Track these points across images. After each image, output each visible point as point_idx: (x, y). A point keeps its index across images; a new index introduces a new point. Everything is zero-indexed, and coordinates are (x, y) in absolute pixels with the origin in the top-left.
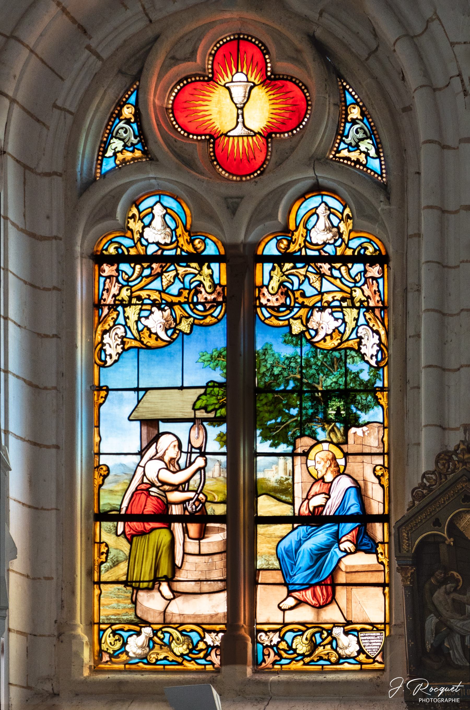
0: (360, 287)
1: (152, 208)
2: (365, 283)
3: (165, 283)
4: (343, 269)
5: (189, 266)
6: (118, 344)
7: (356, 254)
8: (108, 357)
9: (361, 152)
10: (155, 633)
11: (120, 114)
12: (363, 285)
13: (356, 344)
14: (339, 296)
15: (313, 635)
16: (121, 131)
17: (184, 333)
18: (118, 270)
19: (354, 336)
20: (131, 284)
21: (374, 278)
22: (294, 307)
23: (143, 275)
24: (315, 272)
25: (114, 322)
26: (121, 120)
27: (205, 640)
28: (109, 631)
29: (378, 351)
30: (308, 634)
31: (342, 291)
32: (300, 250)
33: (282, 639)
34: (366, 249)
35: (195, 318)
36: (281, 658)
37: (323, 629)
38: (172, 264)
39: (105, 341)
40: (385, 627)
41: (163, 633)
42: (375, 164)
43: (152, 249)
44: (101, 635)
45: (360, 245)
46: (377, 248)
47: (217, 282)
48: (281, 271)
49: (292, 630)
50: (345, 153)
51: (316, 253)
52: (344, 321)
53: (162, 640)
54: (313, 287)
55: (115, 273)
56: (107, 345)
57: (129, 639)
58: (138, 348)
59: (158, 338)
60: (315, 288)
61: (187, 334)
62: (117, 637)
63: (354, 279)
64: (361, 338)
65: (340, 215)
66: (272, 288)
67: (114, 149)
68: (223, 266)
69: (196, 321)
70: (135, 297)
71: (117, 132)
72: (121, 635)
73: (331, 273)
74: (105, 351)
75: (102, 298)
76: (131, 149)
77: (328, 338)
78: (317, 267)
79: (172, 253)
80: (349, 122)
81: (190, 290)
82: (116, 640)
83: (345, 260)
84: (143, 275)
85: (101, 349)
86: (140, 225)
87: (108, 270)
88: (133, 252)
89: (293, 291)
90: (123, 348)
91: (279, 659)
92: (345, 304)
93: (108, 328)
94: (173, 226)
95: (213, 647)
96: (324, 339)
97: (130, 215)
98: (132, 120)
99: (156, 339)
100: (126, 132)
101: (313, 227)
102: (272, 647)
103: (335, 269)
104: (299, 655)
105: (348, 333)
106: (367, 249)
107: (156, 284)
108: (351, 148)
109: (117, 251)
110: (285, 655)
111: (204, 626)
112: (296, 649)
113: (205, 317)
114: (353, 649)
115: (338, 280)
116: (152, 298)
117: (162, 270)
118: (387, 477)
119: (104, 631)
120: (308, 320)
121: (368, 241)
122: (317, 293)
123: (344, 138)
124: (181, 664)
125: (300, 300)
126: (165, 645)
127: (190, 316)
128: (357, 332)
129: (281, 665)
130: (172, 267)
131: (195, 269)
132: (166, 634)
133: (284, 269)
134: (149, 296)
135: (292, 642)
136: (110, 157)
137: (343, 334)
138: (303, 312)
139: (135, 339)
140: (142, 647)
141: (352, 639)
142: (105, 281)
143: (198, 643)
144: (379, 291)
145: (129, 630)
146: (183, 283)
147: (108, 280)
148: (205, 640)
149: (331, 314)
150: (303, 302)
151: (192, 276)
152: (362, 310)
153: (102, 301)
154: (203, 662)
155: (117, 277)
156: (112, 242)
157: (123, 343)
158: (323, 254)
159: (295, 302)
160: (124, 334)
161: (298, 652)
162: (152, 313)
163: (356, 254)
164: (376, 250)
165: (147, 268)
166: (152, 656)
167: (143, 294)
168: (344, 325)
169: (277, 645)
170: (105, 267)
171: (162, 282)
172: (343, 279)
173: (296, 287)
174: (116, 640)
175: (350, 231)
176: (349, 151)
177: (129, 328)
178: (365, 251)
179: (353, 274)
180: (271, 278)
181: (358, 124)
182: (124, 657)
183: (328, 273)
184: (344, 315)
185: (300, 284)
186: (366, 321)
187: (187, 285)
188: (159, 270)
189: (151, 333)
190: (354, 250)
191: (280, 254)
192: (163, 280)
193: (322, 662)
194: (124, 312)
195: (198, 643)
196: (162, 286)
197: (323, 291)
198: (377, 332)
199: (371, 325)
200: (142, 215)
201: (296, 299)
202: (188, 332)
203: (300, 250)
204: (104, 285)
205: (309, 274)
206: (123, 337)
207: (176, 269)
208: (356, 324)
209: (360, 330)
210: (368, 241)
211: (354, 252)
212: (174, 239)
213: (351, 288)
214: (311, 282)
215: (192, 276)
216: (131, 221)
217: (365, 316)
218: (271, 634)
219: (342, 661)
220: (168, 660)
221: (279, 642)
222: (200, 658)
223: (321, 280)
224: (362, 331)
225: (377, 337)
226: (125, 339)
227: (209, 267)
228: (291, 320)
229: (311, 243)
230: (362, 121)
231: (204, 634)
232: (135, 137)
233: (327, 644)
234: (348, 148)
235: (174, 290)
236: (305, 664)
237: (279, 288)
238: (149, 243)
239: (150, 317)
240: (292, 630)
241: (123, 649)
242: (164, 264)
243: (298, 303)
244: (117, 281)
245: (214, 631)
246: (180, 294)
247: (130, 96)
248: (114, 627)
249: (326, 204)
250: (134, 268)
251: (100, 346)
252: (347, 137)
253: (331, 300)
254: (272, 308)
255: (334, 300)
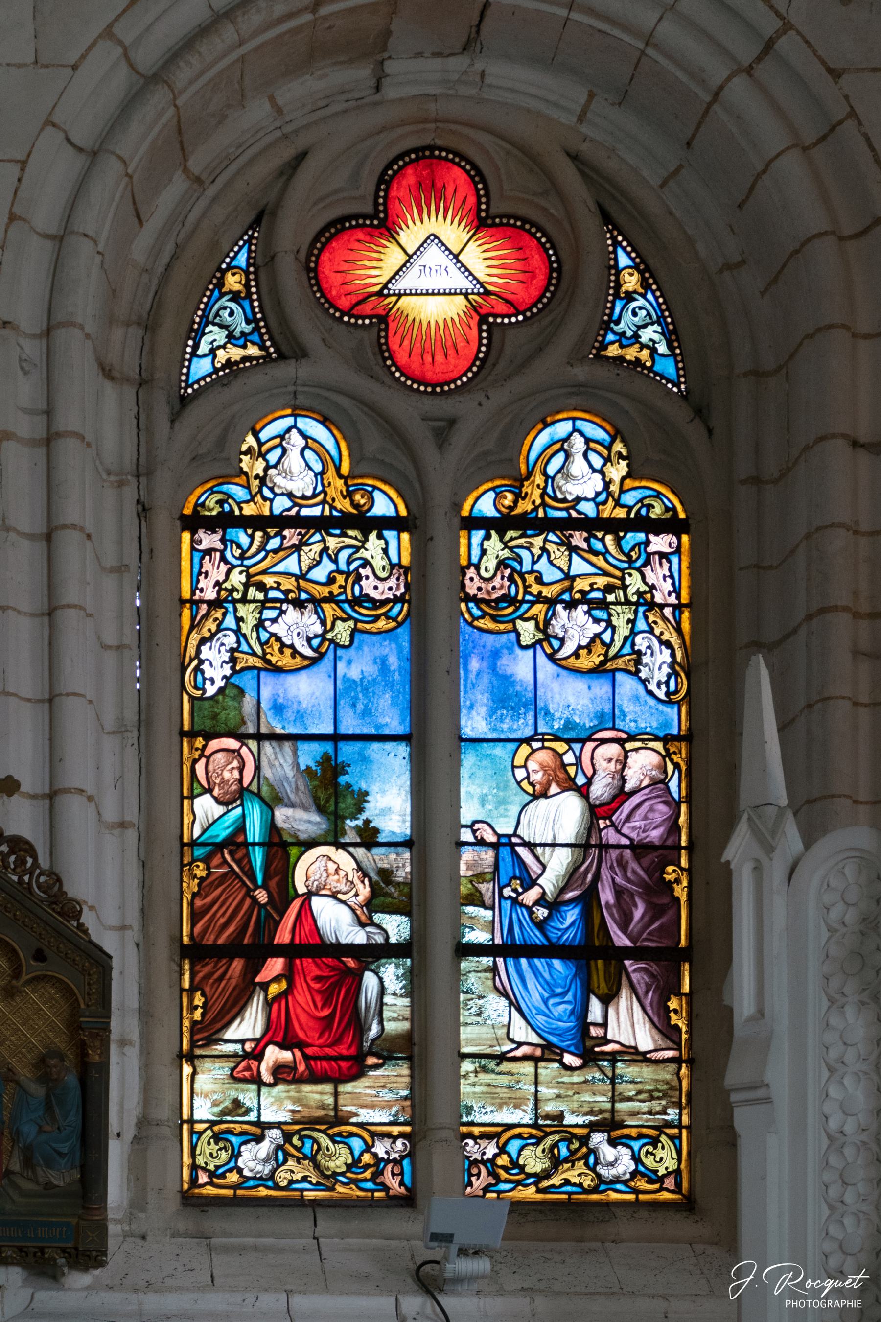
0: (638, 570)
1: (282, 437)
2: (647, 562)
3: (306, 563)
4: (609, 538)
5: (347, 536)
6: (224, 662)
7: (632, 515)
8: (208, 683)
9: (643, 346)
10: (287, 1137)
11: (221, 284)
12: (645, 565)
13: (632, 663)
14: (601, 581)
15: (555, 1145)
16: (225, 314)
17: (337, 645)
18: (223, 540)
19: (627, 649)
20: (246, 562)
21: (663, 555)
22: (523, 601)
23: (268, 548)
24: (557, 540)
25: (219, 626)
26: (222, 295)
27: (373, 1150)
28: (209, 1133)
29: (669, 676)
30: (549, 1141)
31: (606, 574)
32: (536, 509)
33: (502, 1150)
34: (650, 507)
35: (357, 621)
36: (498, 1180)
37: (574, 1136)
38: (318, 530)
39: (202, 656)
40: (681, 1133)
41: (301, 1139)
42: (667, 367)
43: (281, 504)
44: (195, 1140)
45: (641, 501)
46: (670, 505)
47: (395, 560)
48: (501, 540)
49: (519, 1136)
50: (613, 351)
51: (564, 514)
52: (609, 624)
53: (299, 1149)
54: (555, 565)
55: (219, 546)
56: (207, 663)
57: (243, 1148)
58: (259, 669)
59: (295, 653)
60: (559, 568)
61: (344, 647)
62: (221, 1145)
63: (628, 555)
64: (639, 653)
65: (605, 453)
66: (486, 570)
67: (212, 343)
68: (405, 536)
69: (360, 625)
70: (253, 585)
71: (217, 314)
72: (227, 1140)
73: (589, 546)
74: (203, 672)
75: (197, 588)
76: (241, 342)
77: (583, 652)
78: (564, 535)
79: (316, 511)
80: (622, 299)
81: (348, 574)
82: (220, 1149)
83: (614, 526)
84: (268, 548)
85: (197, 669)
86: (260, 465)
87: (209, 540)
88: (249, 510)
89: (522, 575)
90: (233, 668)
91: (493, 1182)
92: (611, 598)
93: (207, 635)
94: (318, 467)
95: (388, 1161)
96: (576, 654)
97: (244, 448)
98: (243, 295)
99: (293, 656)
100: (231, 314)
101: (559, 472)
102: (483, 1162)
103: (596, 537)
104: (529, 1176)
105: (618, 643)
106: (653, 507)
107: (291, 564)
108: (624, 342)
109: (222, 506)
110: (503, 1174)
111: (373, 1128)
112: (525, 1165)
113: (377, 618)
114: (626, 1165)
115: (601, 557)
116: (282, 588)
117: (300, 541)
118: (685, 883)
119: (200, 1134)
120: (547, 623)
121: (655, 493)
122: (562, 576)
123: (612, 325)
124: (332, 1189)
125: (535, 589)
126: (305, 1157)
127: (350, 618)
128: (633, 644)
129: (499, 1192)
130: (317, 537)
131: (356, 538)
132: (306, 1140)
133: (507, 537)
134: (279, 584)
135: (519, 1155)
136: (205, 356)
137: (608, 646)
138: (539, 609)
139: (254, 654)
140: (266, 1160)
141: (625, 1154)
142: (202, 558)
143: (361, 1154)
144: (671, 576)
145: (241, 1134)
146: (335, 561)
147: (207, 558)
148: (373, 1150)
149: (588, 612)
150: (540, 593)
151: (351, 551)
152: (641, 609)
153: (198, 592)
154: (370, 1185)
155: (222, 553)
156: (213, 493)
157: (233, 660)
158: (574, 514)
159: (526, 592)
160: (235, 646)
161: (527, 1170)
162: (283, 612)
163: (632, 515)
164: (667, 509)
165: (276, 535)
166: (282, 1174)
167: (269, 581)
168: (609, 631)
169: (492, 1161)
170: (201, 534)
171: (299, 561)
172: (608, 556)
173: (527, 567)
174: (220, 1149)
175: (623, 479)
176: (622, 346)
177: (244, 636)
178: (648, 511)
179: (626, 549)
180: (484, 552)
181: (636, 300)
182: (233, 1178)
183: (584, 546)
184: (610, 615)
185: (534, 563)
186: (649, 625)
187: (343, 566)
188: (295, 541)
189: (283, 645)
190: (630, 508)
191: (498, 515)
192: (302, 558)
193: (568, 1189)
194: (235, 610)
195: (361, 1154)
196: (300, 567)
197: (572, 574)
198: (668, 644)
199: (657, 632)
200: (264, 449)
201: (526, 587)
202: (347, 643)
203: (536, 509)
204: (201, 566)
205: (550, 547)
206: (232, 650)
207: (323, 540)
208: (632, 630)
209: (638, 639)
210: (655, 493)
211: (628, 513)
212: (319, 488)
213: (622, 570)
214: (552, 558)
215: (351, 551)
216: (246, 459)
217: (646, 618)
218: (483, 1143)
219: (602, 1187)
220: (310, 1183)
221: (496, 1156)
222: (365, 1180)
223: (570, 556)
224: (641, 642)
225: (667, 652)
226: (236, 654)
227: (380, 537)
228: (518, 622)
229: (555, 499)
230: (644, 296)
231: (373, 1142)
232: (248, 322)
233: (579, 1159)
234: (619, 341)
235: (320, 574)
236: (539, 1191)
237: (497, 568)
238: (276, 495)
239: (280, 620)
240: (519, 1136)
241: (232, 1164)
242: (303, 531)
243: (531, 594)
244: (223, 559)
245: (389, 1136)
246: (331, 581)
247: (237, 253)
248: (216, 1128)
249: (582, 434)
250: (252, 537)
251: (195, 662)
252: (617, 322)
253: (587, 588)
254: (487, 602)
255: (592, 590)
